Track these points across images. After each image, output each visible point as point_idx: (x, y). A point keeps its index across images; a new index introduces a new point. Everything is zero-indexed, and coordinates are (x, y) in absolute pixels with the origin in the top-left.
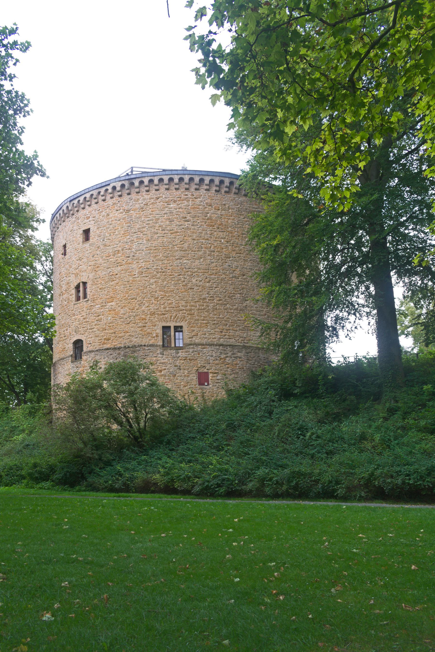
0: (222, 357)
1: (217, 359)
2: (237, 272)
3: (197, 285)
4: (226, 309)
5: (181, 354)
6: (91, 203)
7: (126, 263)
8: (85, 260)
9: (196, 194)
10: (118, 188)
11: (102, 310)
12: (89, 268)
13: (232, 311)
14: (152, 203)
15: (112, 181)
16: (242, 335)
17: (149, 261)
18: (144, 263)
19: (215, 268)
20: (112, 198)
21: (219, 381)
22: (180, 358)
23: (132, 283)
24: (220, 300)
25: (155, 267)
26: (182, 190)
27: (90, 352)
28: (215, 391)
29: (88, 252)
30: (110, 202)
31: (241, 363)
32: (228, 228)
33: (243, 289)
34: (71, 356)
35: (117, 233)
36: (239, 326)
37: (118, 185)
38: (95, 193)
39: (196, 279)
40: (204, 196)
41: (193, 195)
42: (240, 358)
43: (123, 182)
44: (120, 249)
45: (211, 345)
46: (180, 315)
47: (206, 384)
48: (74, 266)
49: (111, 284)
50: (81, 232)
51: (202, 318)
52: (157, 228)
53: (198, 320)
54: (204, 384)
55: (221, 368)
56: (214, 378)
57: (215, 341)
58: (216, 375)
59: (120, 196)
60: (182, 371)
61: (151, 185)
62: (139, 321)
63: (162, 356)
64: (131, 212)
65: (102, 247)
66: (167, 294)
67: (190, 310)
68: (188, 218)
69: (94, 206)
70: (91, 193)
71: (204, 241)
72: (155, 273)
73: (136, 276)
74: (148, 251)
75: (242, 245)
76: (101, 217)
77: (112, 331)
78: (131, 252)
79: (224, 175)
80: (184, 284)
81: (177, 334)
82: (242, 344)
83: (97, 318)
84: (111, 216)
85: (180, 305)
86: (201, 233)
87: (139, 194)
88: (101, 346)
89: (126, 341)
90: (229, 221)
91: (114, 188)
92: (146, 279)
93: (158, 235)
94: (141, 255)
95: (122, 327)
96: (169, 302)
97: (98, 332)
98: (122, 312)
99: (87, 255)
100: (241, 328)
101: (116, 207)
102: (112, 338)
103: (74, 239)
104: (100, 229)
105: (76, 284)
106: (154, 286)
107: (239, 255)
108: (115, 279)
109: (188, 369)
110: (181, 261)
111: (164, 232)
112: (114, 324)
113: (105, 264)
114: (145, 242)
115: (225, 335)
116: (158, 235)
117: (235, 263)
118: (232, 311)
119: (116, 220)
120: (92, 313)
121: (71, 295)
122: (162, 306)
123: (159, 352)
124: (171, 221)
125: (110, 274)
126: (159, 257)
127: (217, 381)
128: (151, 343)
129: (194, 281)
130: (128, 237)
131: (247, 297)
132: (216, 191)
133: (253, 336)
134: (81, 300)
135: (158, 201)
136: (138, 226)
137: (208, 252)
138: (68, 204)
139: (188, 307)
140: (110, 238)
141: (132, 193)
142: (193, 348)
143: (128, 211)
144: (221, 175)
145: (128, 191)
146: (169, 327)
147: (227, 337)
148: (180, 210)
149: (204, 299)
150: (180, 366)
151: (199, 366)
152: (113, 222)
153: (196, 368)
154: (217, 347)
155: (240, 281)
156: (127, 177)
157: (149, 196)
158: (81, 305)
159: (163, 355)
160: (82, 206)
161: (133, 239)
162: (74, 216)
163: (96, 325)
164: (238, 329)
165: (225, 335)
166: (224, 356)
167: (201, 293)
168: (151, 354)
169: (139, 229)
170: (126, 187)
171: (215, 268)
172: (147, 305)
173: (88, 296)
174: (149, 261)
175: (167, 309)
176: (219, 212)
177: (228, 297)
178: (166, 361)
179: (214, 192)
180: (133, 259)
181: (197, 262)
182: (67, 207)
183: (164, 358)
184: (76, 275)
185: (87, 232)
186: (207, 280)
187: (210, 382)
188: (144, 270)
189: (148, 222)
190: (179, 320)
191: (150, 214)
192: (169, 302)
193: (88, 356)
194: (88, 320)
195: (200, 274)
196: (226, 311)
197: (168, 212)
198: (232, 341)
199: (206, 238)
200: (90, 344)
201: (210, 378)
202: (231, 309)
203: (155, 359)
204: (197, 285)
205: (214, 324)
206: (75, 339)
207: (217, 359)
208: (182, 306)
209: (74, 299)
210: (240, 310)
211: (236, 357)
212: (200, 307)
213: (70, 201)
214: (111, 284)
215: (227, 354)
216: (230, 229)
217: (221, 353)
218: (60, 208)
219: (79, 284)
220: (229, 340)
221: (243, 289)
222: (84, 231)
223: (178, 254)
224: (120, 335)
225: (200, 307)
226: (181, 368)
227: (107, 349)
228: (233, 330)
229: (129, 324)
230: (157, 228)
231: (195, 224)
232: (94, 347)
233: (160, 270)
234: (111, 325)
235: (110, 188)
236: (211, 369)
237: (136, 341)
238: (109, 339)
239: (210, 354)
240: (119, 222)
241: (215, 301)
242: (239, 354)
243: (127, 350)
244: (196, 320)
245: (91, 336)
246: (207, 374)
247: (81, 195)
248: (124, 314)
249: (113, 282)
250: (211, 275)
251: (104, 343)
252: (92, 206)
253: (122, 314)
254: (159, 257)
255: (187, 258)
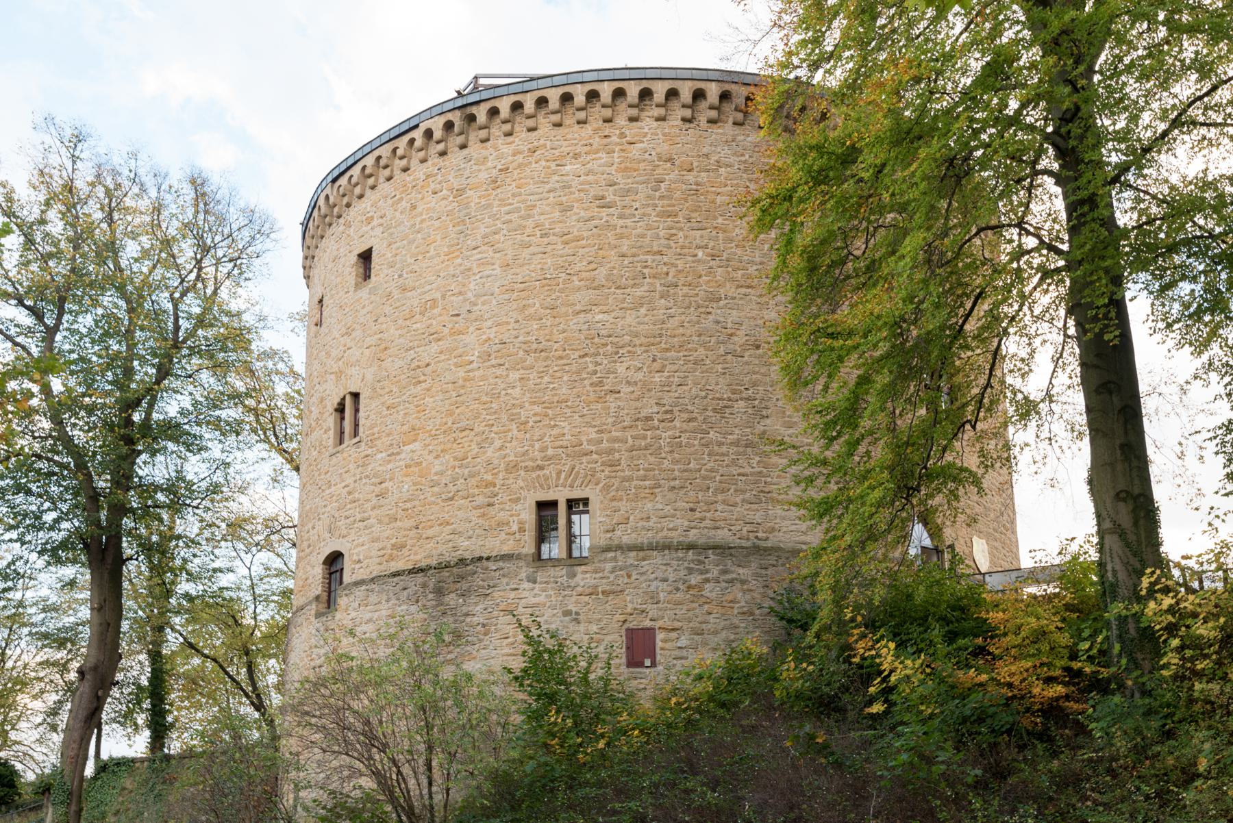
0: (693, 582)
1: (677, 589)
2: (740, 339)
3: (628, 382)
4: (706, 445)
5: (584, 578)
6: (377, 180)
7: (453, 333)
8: (358, 333)
9: (632, 131)
10: (438, 134)
11: (389, 466)
12: (367, 352)
13: (724, 449)
14: (519, 166)
15: (423, 117)
16: (750, 516)
17: (508, 323)
18: (494, 329)
19: (681, 330)
20: (423, 161)
21: (684, 653)
22: (579, 589)
23: (463, 386)
24: (690, 420)
25: (521, 338)
26: (595, 126)
27: (357, 584)
28: (646, 687)
29: (365, 311)
30: (419, 171)
31: (748, 597)
32: (715, 218)
33: (755, 384)
34: (317, 598)
35: (432, 252)
36: (743, 492)
37: (437, 125)
38: (385, 151)
39: (625, 365)
40: (653, 135)
41: (622, 135)
42: (743, 582)
43: (450, 116)
44: (438, 295)
45: (666, 547)
46: (583, 465)
47: (648, 662)
48: (334, 353)
49: (414, 391)
50: (353, 258)
51: (642, 472)
52: (528, 231)
53: (630, 479)
54: (640, 664)
55: (691, 614)
56: (668, 645)
57: (675, 536)
58: (674, 635)
59: (443, 154)
60: (582, 627)
61: (518, 119)
62: (476, 491)
63: (531, 585)
64: (470, 193)
65: (396, 294)
66: (550, 412)
67: (610, 451)
68: (610, 198)
69: (384, 187)
70: (376, 153)
71: (649, 258)
72: (521, 353)
73: (475, 365)
74: (507, 297)
75: (752, 262)
76: (397, 214)
77: (412, 523)
78: (465, 300)
79: (704, 75)
80: (595, 379)
81: (575, 518)
82: (749, 544)
83: (377, 489)
84: (419, 209)
85: (584, 438)
86: (643, 236)
87: (488, 144)
88: (382, 568)
89: (442, 549)
90: (719, 199)
91: (429, 134)
92: (499, 371)
93: (533, 249)
94: (486, 307)
95: (435, 508)
96: (555, 432)
97: (377, 528)
98: (438, 468)
99: (362, 320)
100: (747, 495)
101: (433, 186)
102: (409, 542)
103: (339, 280)
104: (394, 246)
105: (337, 400)
106: (517, 392)
107: (743, 290)
108: (422, 378)
109: (600, 620)
110: (589, 316)
111: (546, 240)
112: (417, 503)
113: (402, 340)
114: (498, 271)
115: (703, 519)
116: (533, 249)
117: (734, 312)
118: (724, 449)
119: (431, 218)
120: (367, 477)
121: (325, 432)
122: (537, 446)
123: (523, 575)
124: (566, 209)
125: (413, 366)
126: (532, 310)
127: (677, 653)
128: (506, 549)
129: (621, 369)
130: (459, 261)
131: (766, 408)
132: (684, 120)
133: (783, 518)
134: (346, 443)
135: (532, 159)
136: (483, 230)
137: (659, 288)
138: (328, 191)
139: (605, 445)
140: (416, 267)
141: (470, 143)
142: (615, 559)
143: (461, 191)
144: (696, 74)
145: (460, 140)
146: (553, 504)
147: (708, 523)
148: (590, 178)
149: (649, 419)
150: (577, 614)
151: (629, 610)
152: (424, 225)
153: (622, 618)
154: (680, 554)
155: (747, 363)
156: (460, 102)
157: (513, 146)
158: (345, 455)
159: (535, 582)
160: (358, 190)
161: (469, 265)
162: (342, 220)
163: (373, 508)
164: (738, 500)
165: (703, 519)
166: (700, 578)
167: (639, 404)
168: (505, 580)
169: (485, 237)
170: (456, 129)
171: (681, 330)
172: (498, 444)
173: (361, 434)
174: (508, 323)
175: (550, 452)
176: (690, 177)
177: (714, 410)
178: (542, 599)
179: (679, 122)
180: (467, 320)
181: (630, 319)
182: (327, 197)
183: (536, 591)
184: (339, 374)
185: (366, 257)
186: (657, 365)
187: (658, 657)
188: (495, 348)
189: (507, 217)
190: (578, 482)
191: (514, 195)
192: (555, 432)
193: (352, 598)
194: (357, 495)
195: (639, 350)
196: (707, 450)
197: (557, 185)
198: (722, 535)
199: (655, 249)
200: (359, 561)
201: (659, 644)
202: (720, 444)
203: (513, 595)
204: (628, 382)
205: (674, 487)
206: (327, 551)
207: (677, 589)
208: (589, 442)
209: (331, 442)
210: (747, 446)
211: (731, 581)
212: (637, 443)
213: (334, 181)
214: (414, 391)
215: (707, 571)
216: (720, 220)
217: (690, 571)
218: (314, 206)
219: (344, 399)
220: (713, 532)
221: (755, 384)
222: (360, 256)
223: (582, 298)
224: (430, 532)
225: (637, 443)
226: (581, 617)
227: (396, 574)
228: (724, 502)
229: (451, 499)
230: (528, 231)
231: (627, 211)
232: (368, 570)
233: (535, 346)
234: (409, 505)
235: (418, 134)
236: (658, 617)
237: (468, 547)
238: (403, 546)
239: (659, 574)
240: (437, 224)
241: (677, 423)
242: (741, 571)
243: (445, 573)
244: (625, 479)
245: (361, 540)
246: (650, 632)
247: (355, 163)
248: (441, 473)
249: (419, 387)
250: (667, 350)
251: (392, 558)
252: (379, 187)
253: (436, 474)
254: (532, 310)
255: (605, 308)
